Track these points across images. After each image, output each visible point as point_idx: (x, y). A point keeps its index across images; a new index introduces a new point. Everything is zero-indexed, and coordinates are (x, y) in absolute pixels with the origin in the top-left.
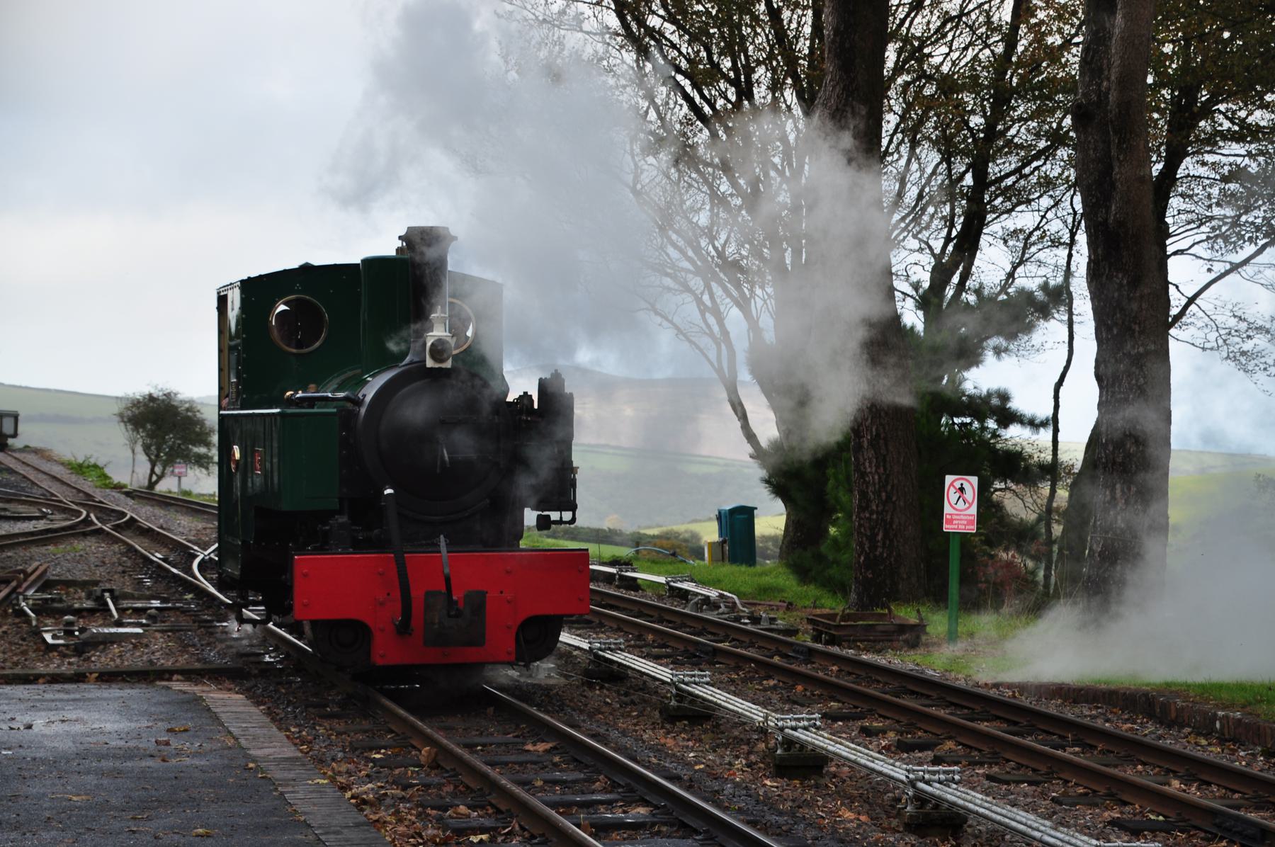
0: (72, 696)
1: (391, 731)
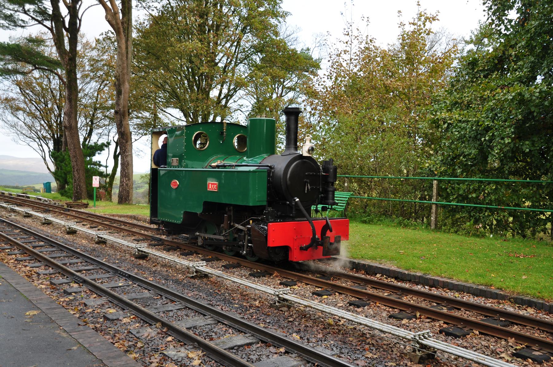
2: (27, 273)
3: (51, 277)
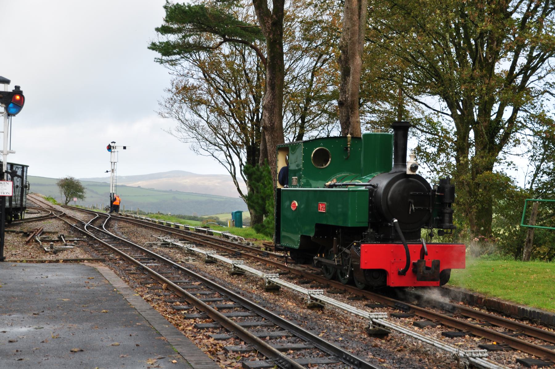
0: (57, 267)
1: (152, 278)
2: (210, 347)
3: (243, 356)
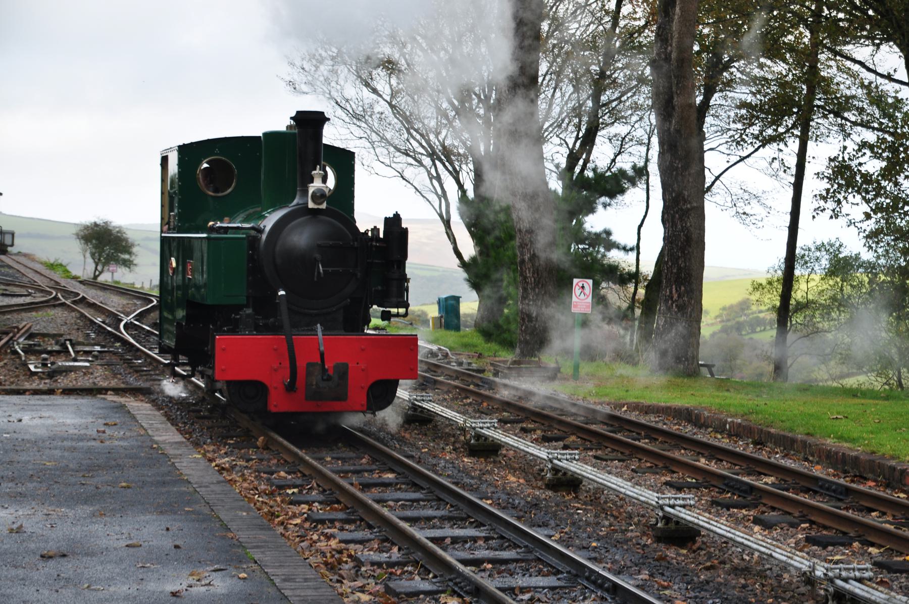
0: (46, 403)
2: (328, 555)
3: (391, 573)
